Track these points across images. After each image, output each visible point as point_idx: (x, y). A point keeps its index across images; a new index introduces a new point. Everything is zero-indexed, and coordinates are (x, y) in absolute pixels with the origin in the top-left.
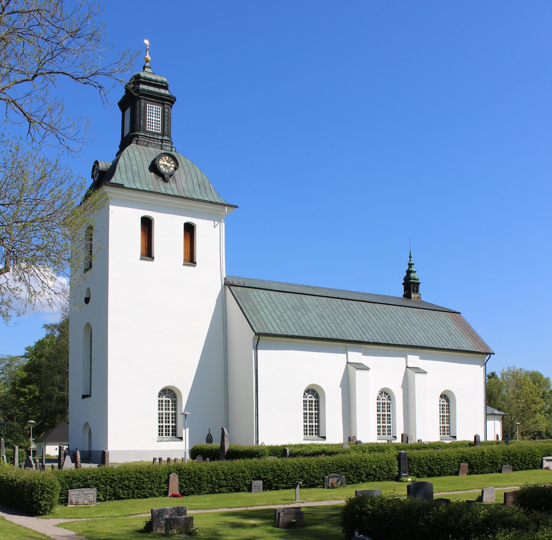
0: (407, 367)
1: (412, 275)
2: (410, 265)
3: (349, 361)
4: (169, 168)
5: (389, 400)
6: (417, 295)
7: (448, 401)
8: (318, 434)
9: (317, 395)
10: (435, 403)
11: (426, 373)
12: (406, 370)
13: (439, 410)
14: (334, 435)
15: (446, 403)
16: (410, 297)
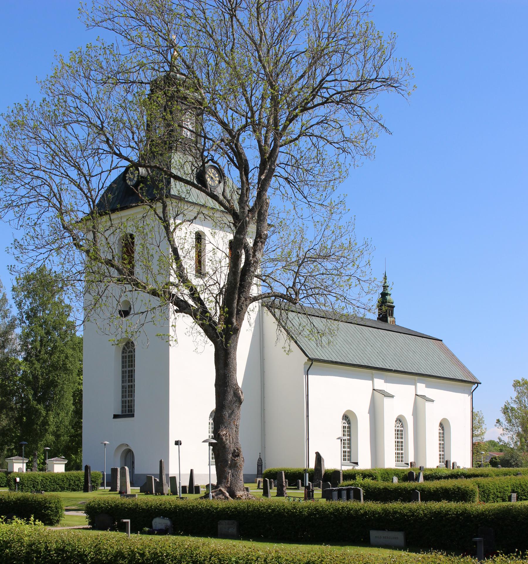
0: (374, 390)
1: (388, 297)
2: (385, 287)
3: (375, 388)
4: (214, 181)
5: (402, 427)
6: (392, 319)
7: (349, 423)
8: (349, 460)
9: (349, 420)
10: (436, 429)
11: (433, 401)
12: (373, 393)
13: (394, 436)
14: (365, 463)
15: (347, 425)
16: (386, 321)
